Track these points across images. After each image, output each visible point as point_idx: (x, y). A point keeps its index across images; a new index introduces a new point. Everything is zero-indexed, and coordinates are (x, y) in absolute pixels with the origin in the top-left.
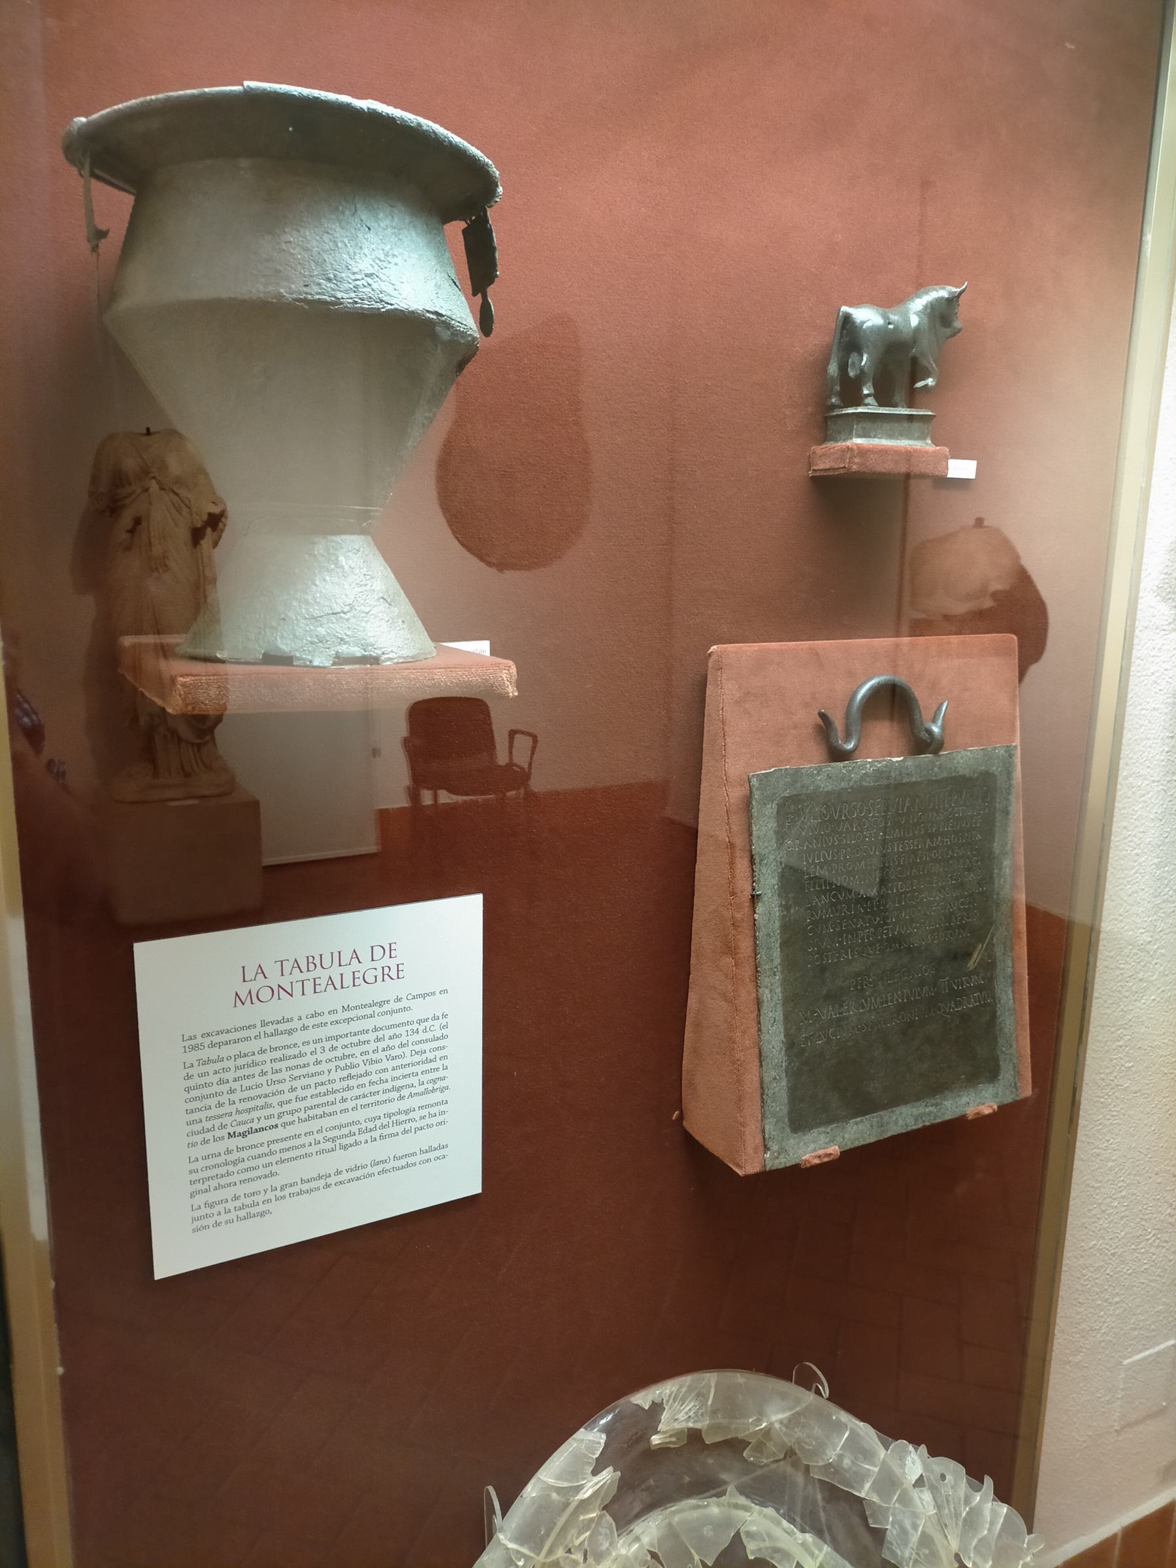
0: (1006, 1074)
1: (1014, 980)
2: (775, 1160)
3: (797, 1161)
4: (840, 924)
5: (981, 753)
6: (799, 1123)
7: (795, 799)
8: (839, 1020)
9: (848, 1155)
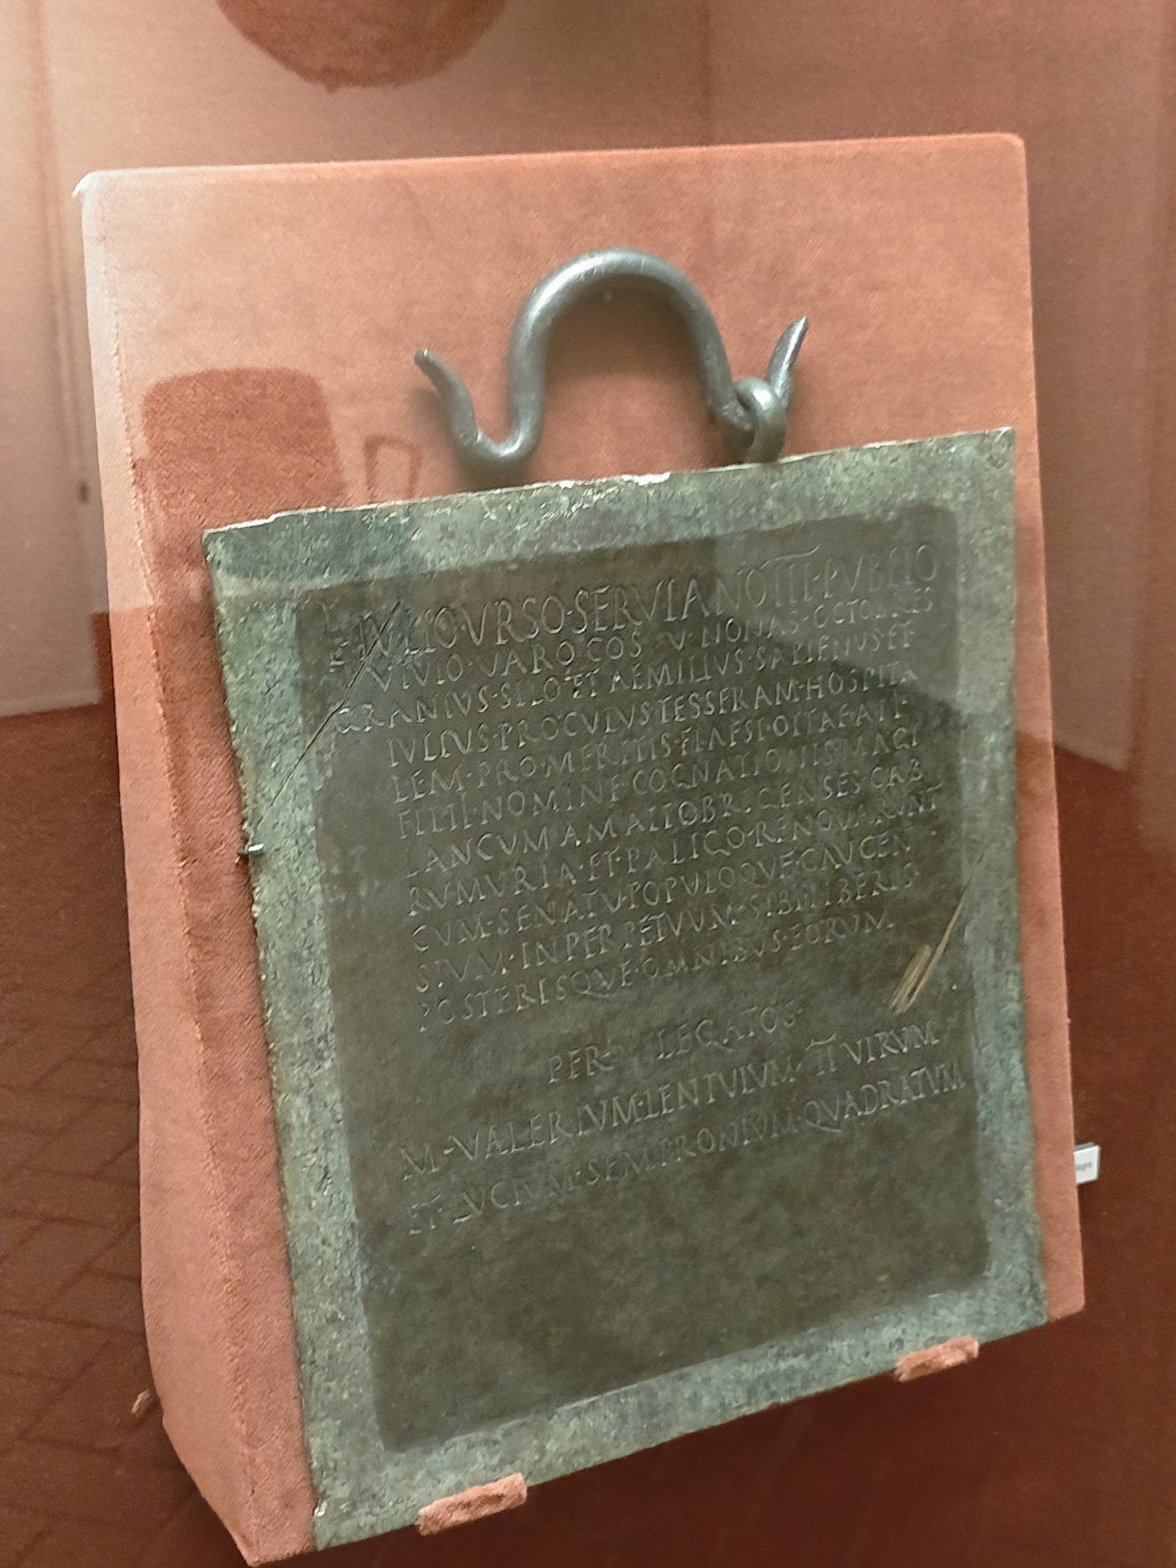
0: (1008, 1263)
1: (1026, 1030)
2: (340, 1521)
3: (408, 1519)
4: (511, 917)
5: (905, 457)
6: (409, 1421)
7: (355, 596)
8: (517, 1161)
9: (550, 1496)
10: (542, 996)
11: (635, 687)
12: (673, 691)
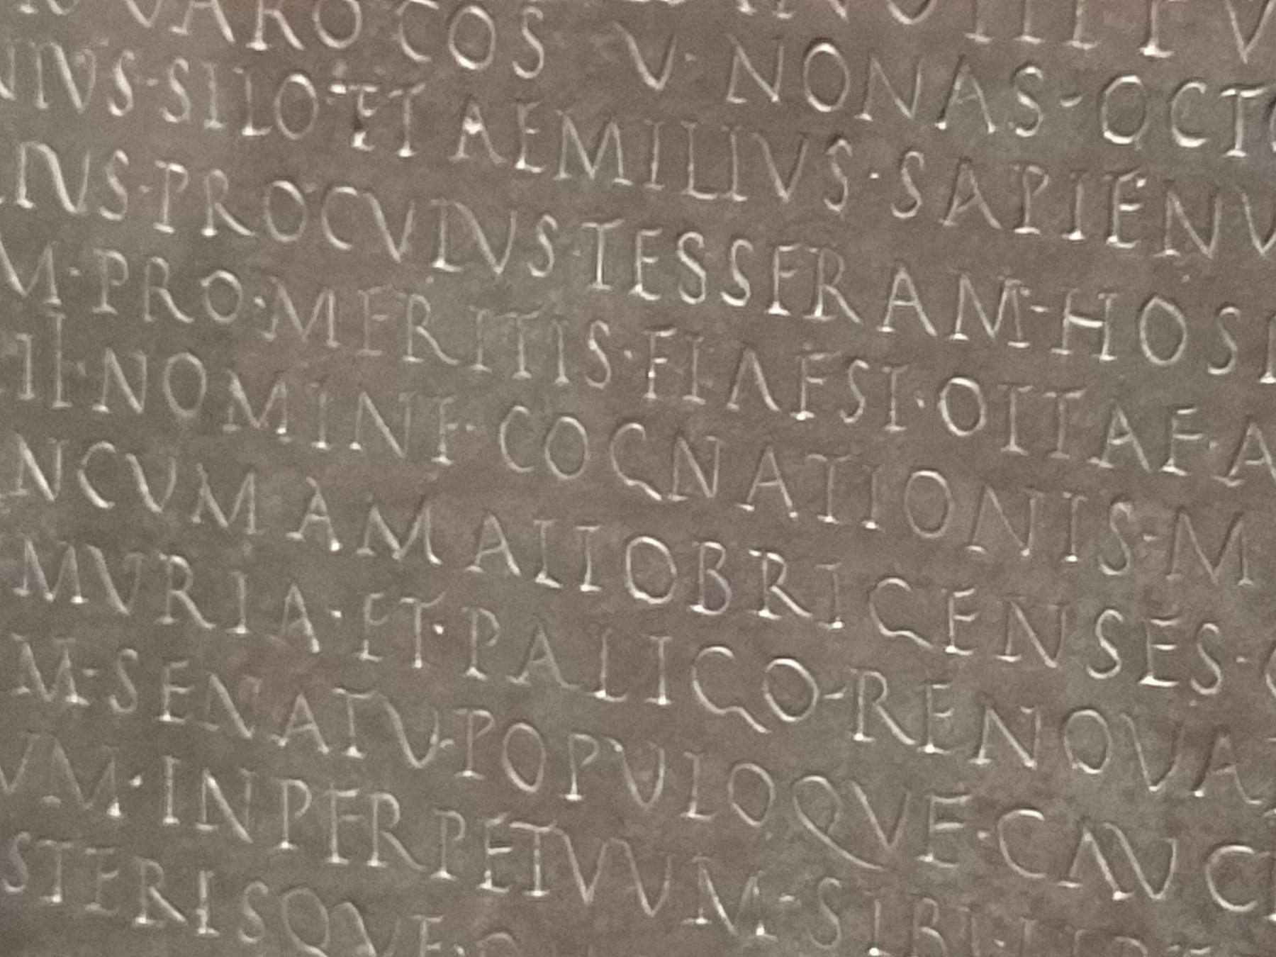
10: (203, 914)
11: (521, 165)
12: (608, 204)
